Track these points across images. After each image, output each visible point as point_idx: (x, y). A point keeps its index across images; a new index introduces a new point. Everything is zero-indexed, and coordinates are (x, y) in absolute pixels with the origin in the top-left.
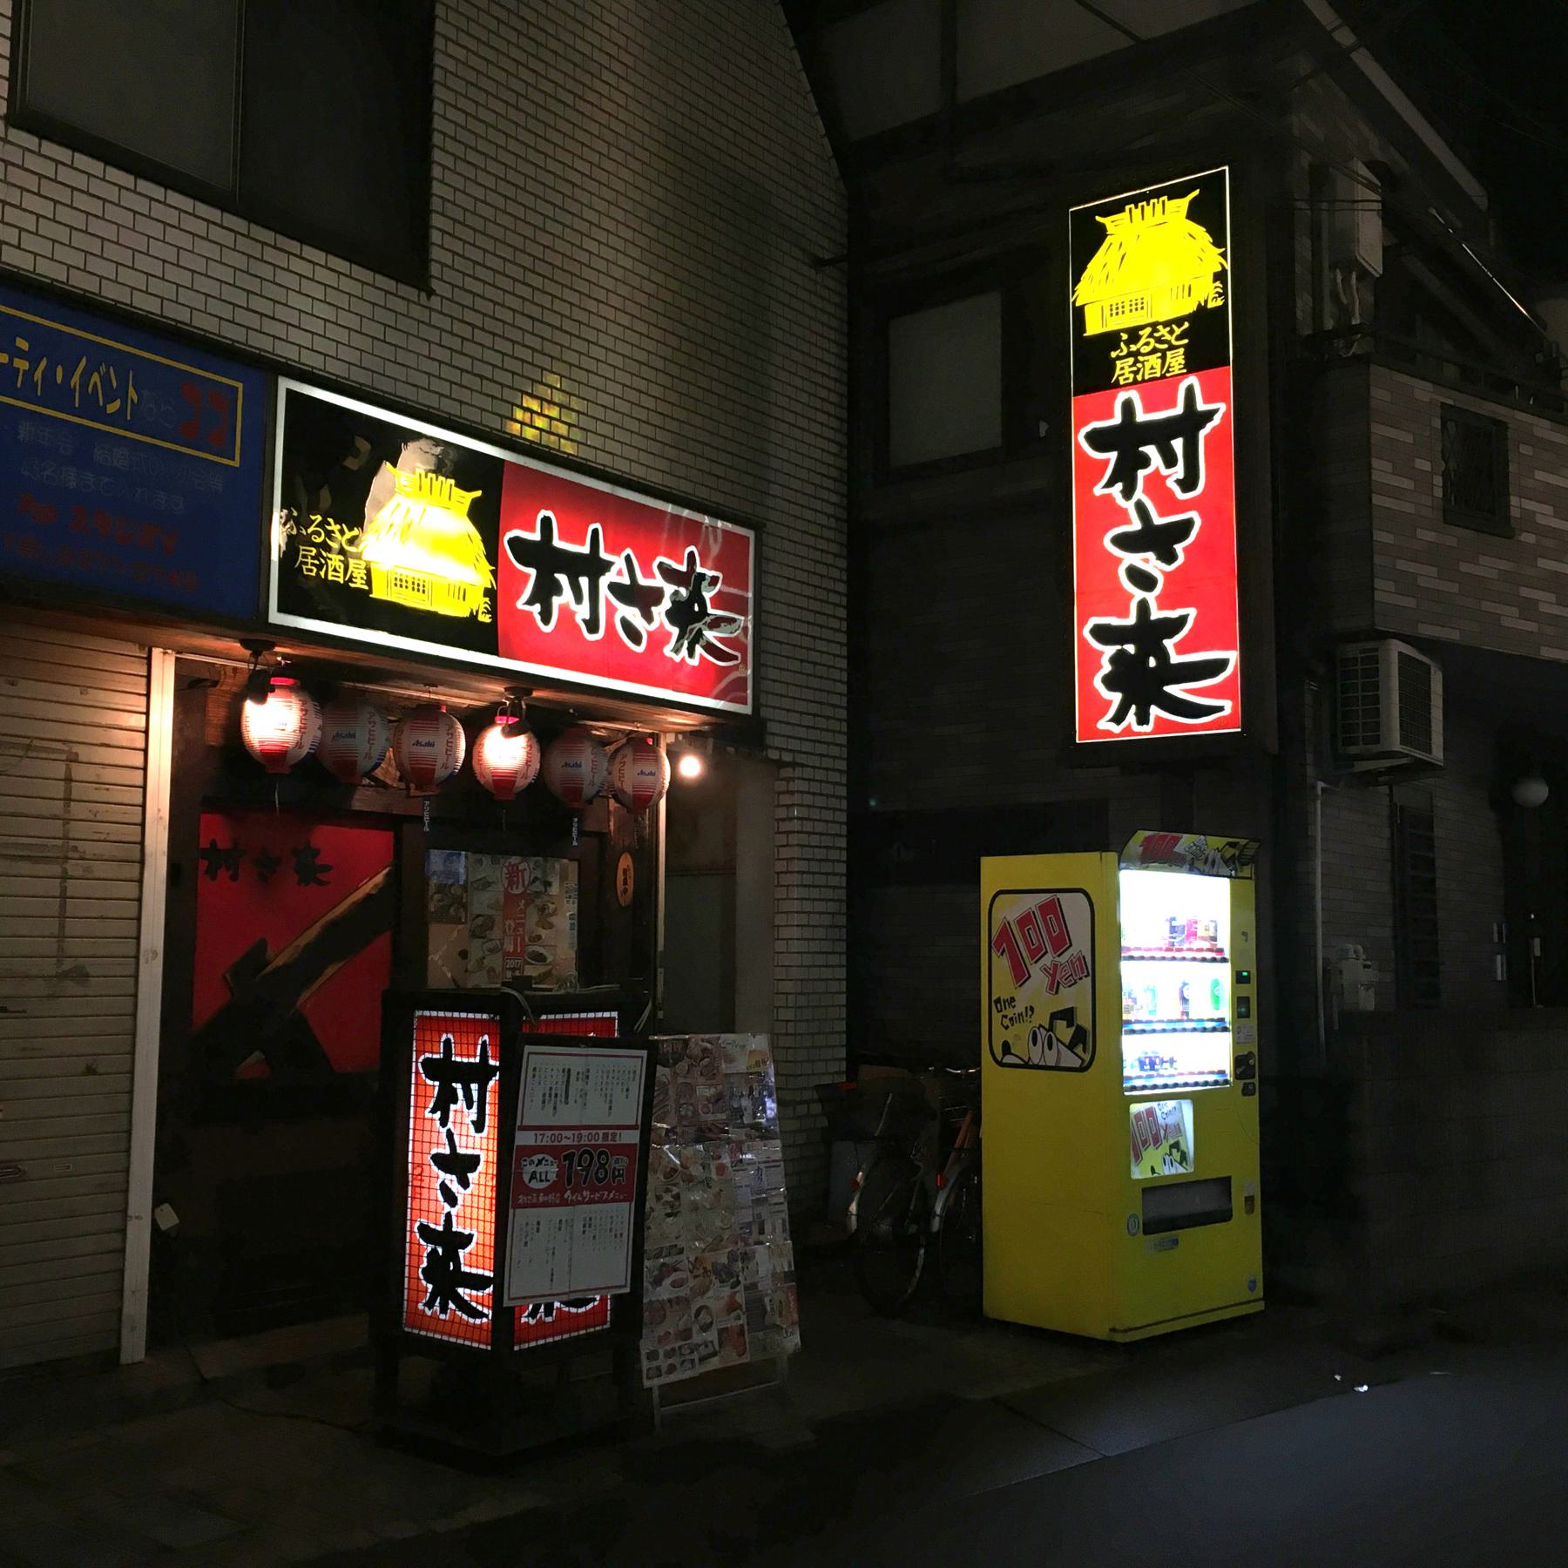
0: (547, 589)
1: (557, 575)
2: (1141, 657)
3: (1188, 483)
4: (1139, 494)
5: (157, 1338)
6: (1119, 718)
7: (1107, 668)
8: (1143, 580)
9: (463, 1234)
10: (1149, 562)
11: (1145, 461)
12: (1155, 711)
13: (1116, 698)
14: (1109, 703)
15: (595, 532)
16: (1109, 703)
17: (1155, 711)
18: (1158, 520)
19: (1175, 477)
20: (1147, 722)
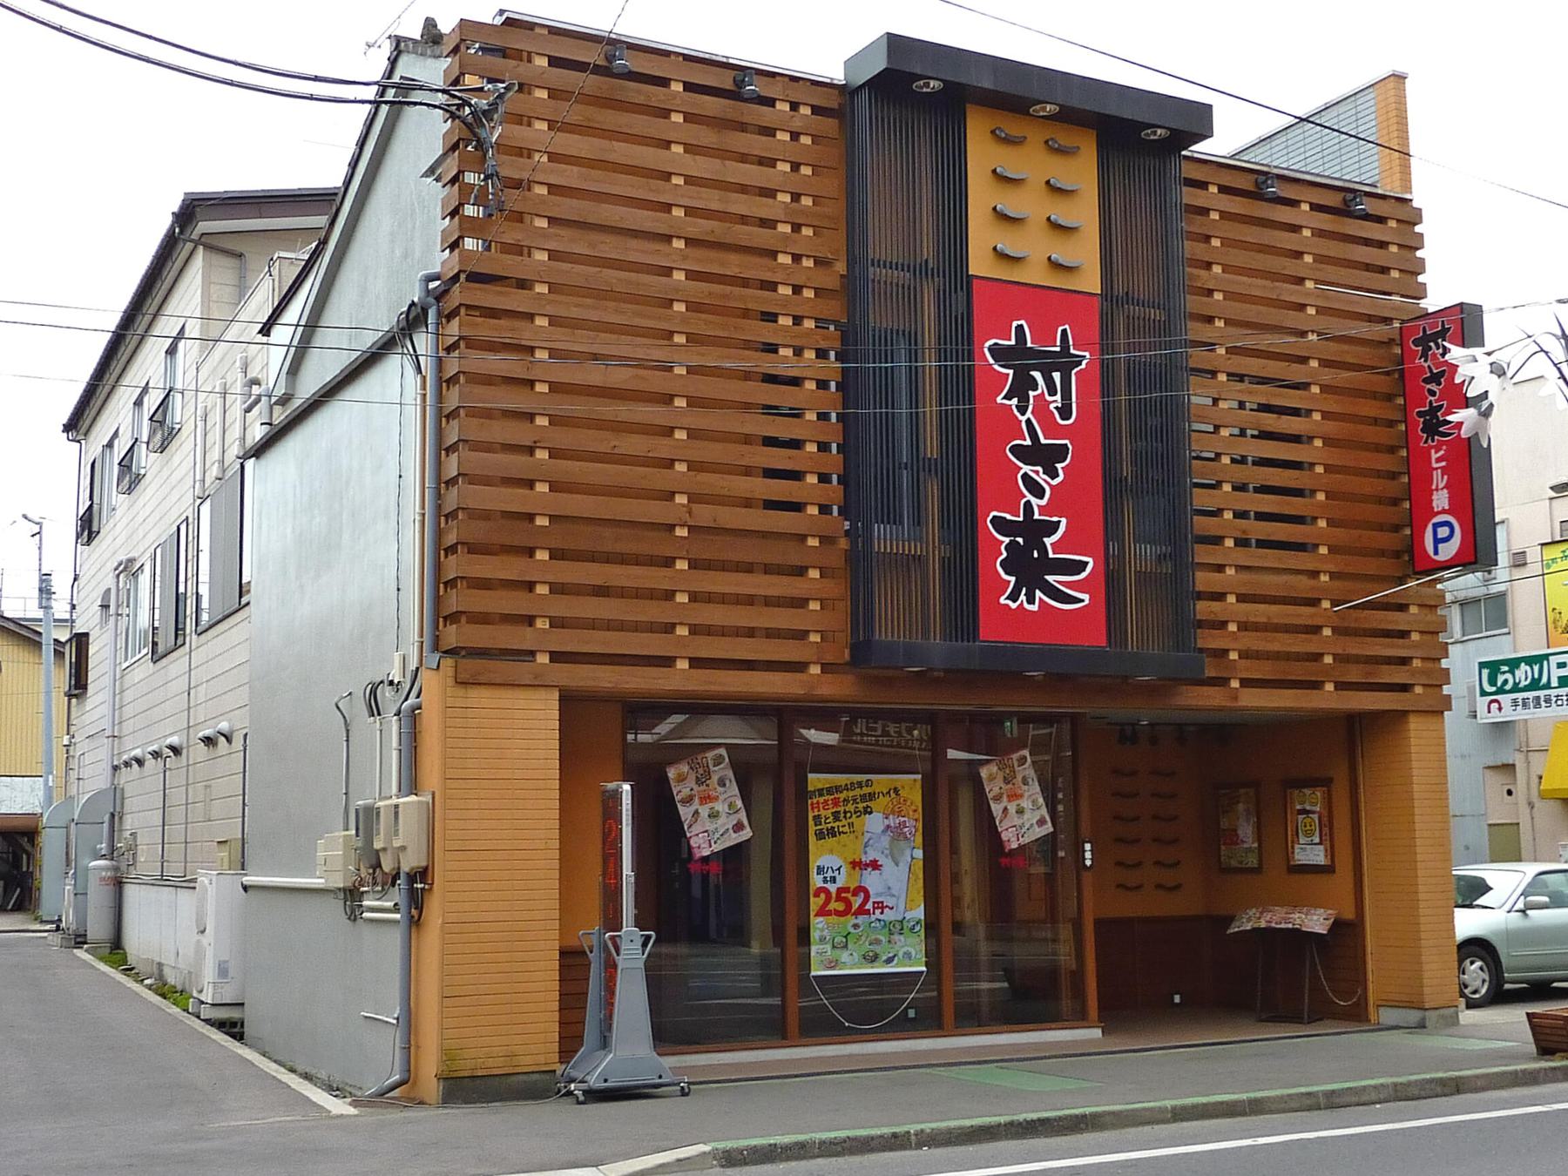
0: (1022, 387)
1: (1032, 373)
2: (1431, 420)
3: (1065, 411)
4: (1029, 414)
5: (1460, 878)
6: (1014, 597)
7: (1421, 426)
8: (1432, 393)
9: (1259, 929)
10: (1433, 387)
11: (1430, 348)
12: (1436, 437)
13: (1425, 435)
14: (1009, 582)
15: (1064, 331)
16: (1009, 582)
17: (1436, 437)
18: (1435, 371)
19: (1055, 405)
20: (1014, 601)
